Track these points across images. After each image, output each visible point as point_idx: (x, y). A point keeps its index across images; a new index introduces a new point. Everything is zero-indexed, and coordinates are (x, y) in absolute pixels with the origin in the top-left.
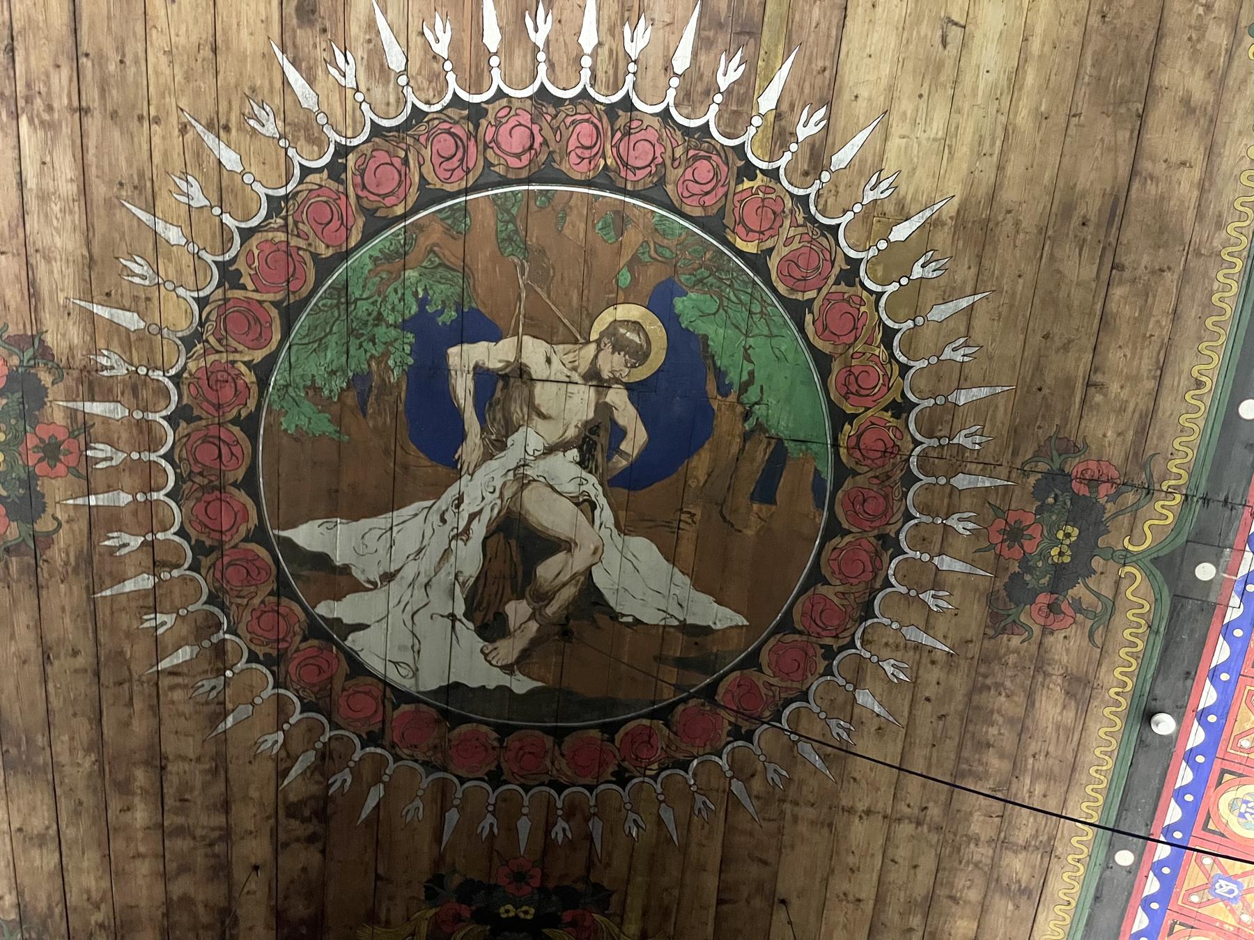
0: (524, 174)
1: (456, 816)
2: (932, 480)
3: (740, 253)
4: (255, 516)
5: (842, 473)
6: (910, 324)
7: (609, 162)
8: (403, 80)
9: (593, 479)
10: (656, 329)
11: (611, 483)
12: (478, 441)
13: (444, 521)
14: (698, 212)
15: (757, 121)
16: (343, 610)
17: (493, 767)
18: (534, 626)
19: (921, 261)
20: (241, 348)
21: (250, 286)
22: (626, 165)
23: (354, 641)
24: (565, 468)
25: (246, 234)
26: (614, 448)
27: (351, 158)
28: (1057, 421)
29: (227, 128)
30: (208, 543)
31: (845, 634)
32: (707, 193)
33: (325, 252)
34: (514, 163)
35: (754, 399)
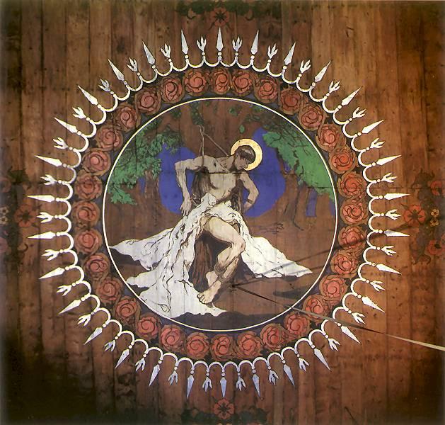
0: (200, 95)
1: (193, 379)
8: (154, 67)
9: (238, 214)
12: (189, 201)
15: (285, 68)
16: (140, 280)
18: (219, 283)
22: (238, 87)
23: (143, 296)
24: (226, 210)
26: (245, 199)
28: (421, 167)
29: (93, 90)
30: (84, 253)
31: (353, 272)
34: (196, 91)
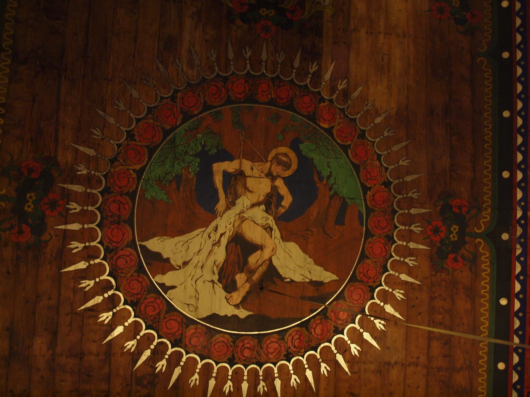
2: (403, 211)
3: (322, 128)
4: (131, 236)
5: (369, 211)
6: (386, 152)
7: (273, 96)
9: (271, 218)
10: (292, 155)
11: (277, 220)
12: (224, 202)
13: (210, 237)
14: (306, 113)
16: (168, 279)
17: (230, 356)
18: (248, 285)
19: (387, 130)
20: (132, 164)
21: (138, 139)
25: (138, 120)
26: (279, 204)
27: (179, 95)
29: (135, 84)
30: (111, 248)
31: (378, 280)
32: (309, 107)
33: (168, 127)
35: (333, 182)
